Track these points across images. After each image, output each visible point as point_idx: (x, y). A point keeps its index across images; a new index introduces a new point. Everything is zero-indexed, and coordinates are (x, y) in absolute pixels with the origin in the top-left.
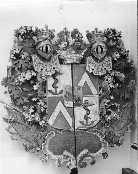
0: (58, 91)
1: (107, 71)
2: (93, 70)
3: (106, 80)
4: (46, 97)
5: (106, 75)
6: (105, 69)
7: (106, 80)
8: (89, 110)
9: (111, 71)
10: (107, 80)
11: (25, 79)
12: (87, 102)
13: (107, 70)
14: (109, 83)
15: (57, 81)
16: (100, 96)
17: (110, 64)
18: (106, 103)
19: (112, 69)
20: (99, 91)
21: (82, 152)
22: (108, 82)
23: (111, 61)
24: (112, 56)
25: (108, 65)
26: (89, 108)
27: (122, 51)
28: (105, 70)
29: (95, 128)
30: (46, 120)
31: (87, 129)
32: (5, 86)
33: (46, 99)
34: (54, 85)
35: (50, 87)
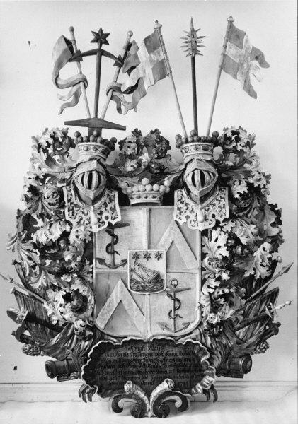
0: (118, 260)
1: (218, 222)
2: (187, 217)
3: (214, 239)
4: (92, 272)
5: (215, 228)
6: (214, 216)
7: (214, 239)
8: (178, 301)
9: (225, 220)
10: (216, 240)
11: (50, 237)
12: (175, 283)
13: (217, 218)
14: (219, 247)
15: (115, 239)
16: (203, 272)
17: (224, 205)
18: (212, 288)
19: (227, 216)
20: (202, 260)
21: (161, 385)
22: (219, 243)
23: (227, 199)
24: (230, 187)
25: (219, 207)
26: (179, 296)
27: (253, 177)
28: (212, 218)
29: (189, 336)
30: (91, 319)
31: (171, 338)
32: (277, 207)
33: (92, 277)
34: (110, 248)
35: (100, 252)
